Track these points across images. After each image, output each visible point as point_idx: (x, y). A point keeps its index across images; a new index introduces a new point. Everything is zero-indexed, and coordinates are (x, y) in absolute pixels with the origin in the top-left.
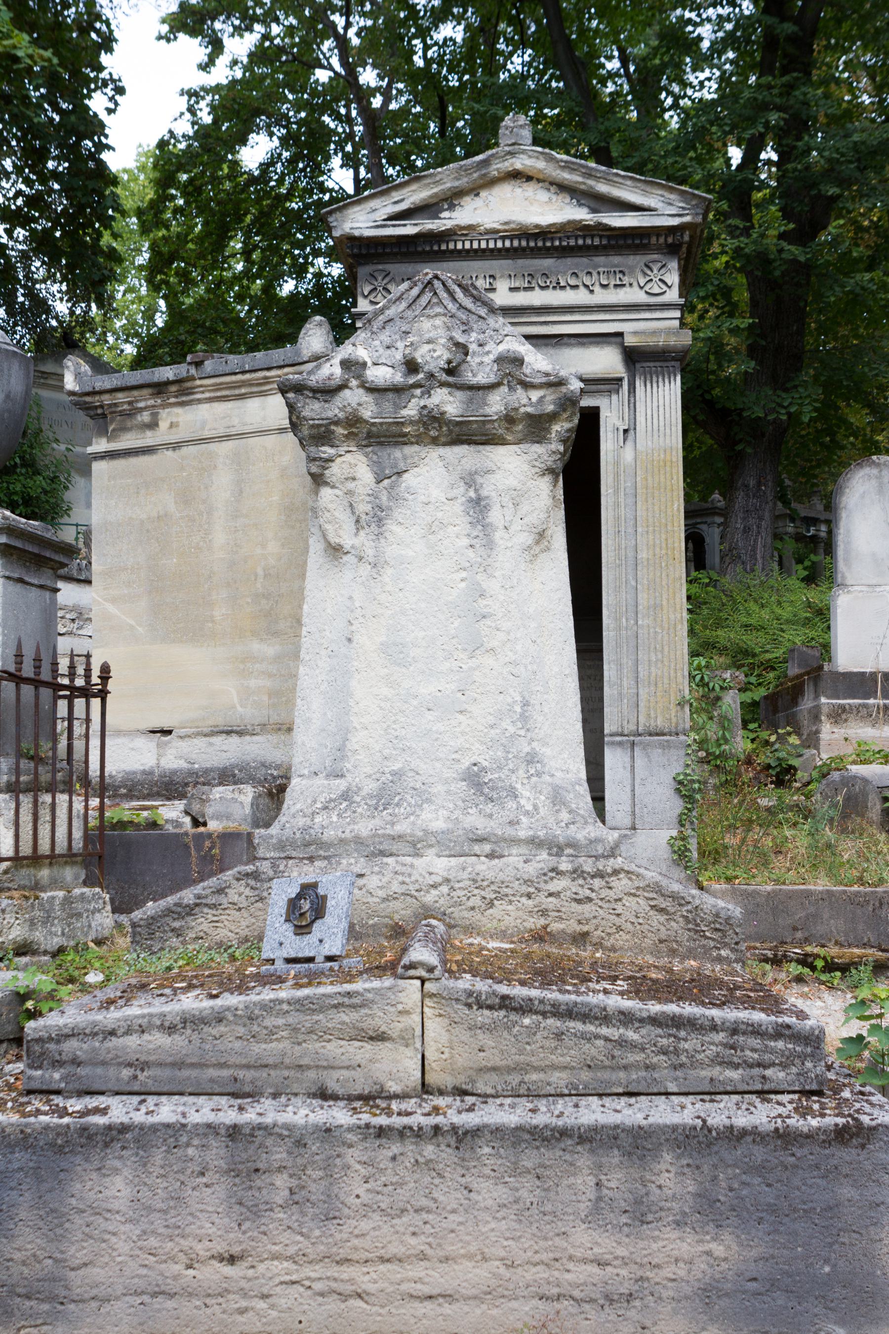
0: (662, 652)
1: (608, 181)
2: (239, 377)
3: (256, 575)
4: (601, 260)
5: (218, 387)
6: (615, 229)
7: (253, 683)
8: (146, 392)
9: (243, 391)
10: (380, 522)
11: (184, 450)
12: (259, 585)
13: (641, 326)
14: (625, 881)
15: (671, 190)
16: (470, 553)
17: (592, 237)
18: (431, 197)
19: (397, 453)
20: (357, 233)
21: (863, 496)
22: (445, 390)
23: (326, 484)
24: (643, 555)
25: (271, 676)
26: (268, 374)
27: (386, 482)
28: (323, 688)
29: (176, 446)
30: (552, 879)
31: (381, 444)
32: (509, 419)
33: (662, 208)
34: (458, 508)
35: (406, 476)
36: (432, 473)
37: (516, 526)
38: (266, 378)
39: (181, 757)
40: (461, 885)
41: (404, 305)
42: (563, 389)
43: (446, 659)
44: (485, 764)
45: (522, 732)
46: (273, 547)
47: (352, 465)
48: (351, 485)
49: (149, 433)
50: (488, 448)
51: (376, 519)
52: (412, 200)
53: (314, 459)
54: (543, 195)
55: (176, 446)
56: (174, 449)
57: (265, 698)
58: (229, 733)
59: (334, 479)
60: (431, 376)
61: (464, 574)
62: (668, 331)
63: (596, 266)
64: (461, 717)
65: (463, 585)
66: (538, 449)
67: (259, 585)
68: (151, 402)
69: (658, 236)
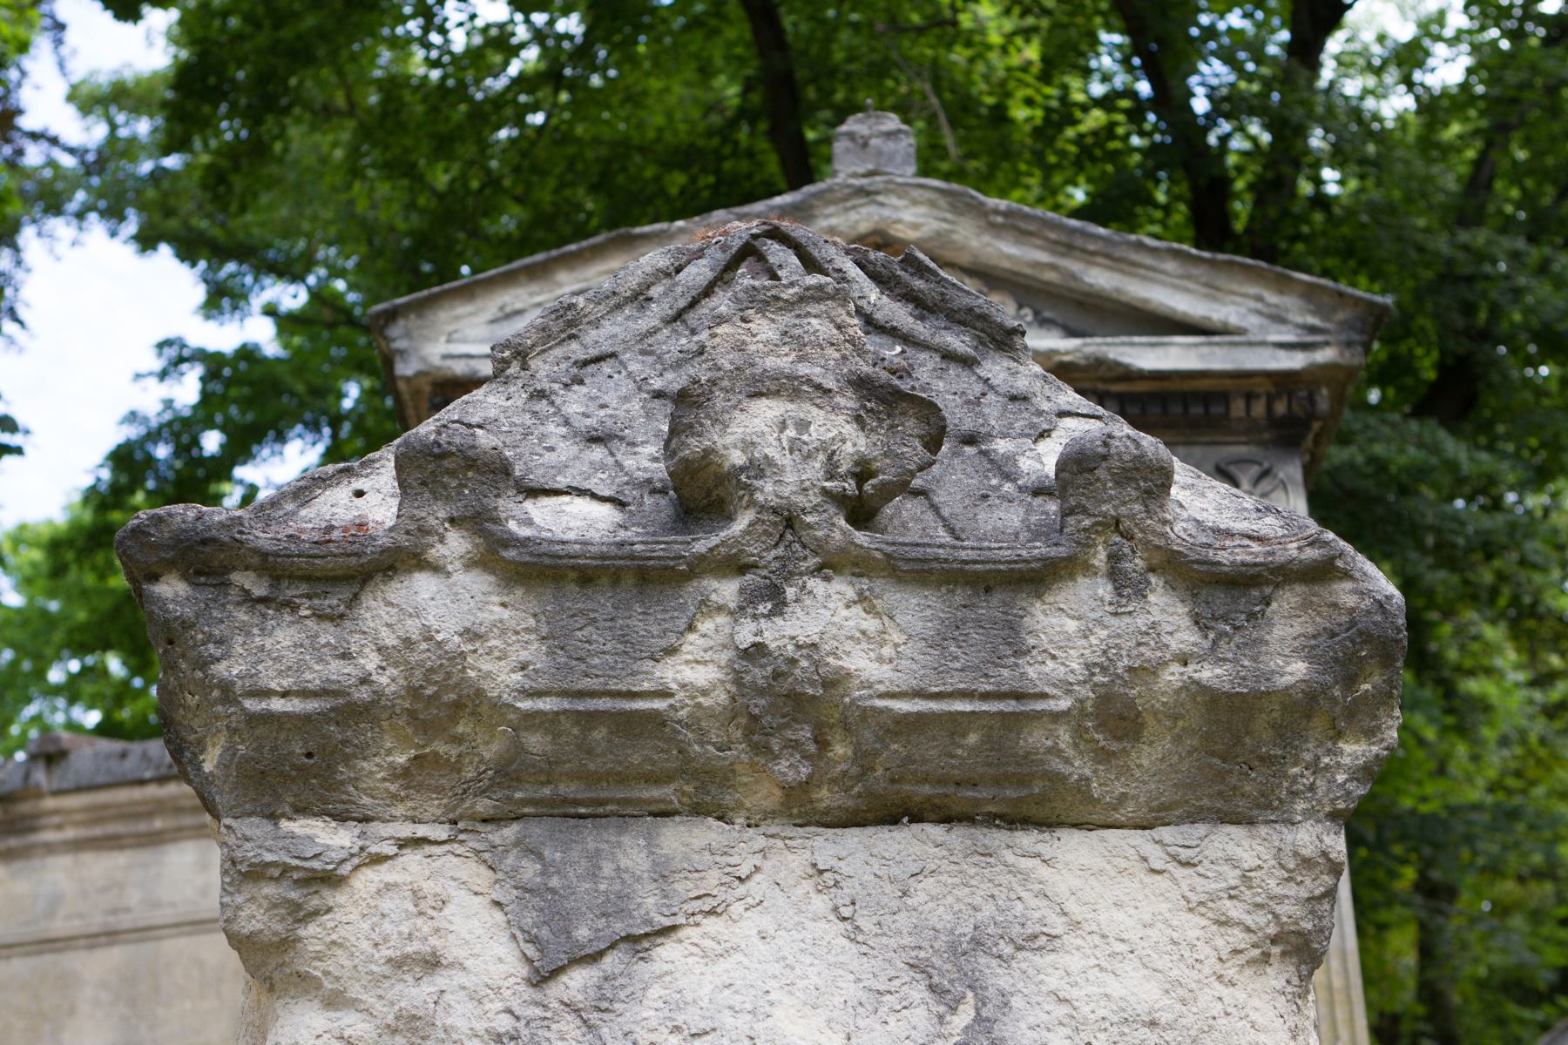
1: (1117, 263)
2: (152, 791)
5: (97, 815)
6: (1143, 376)
9: (158, 824)
19: (631, 853)
22: (843, 587)
23: (305, 985)
27: (577, 981)
31: (564, 811)
32: (1114, 715)
35: (667, 952)
41: (652, 317)
48: (415, 993)
50: (1027, 839)
53: (257, 873)
60: (788, 520)
66: (1240, 847)
69: (1249, 397)
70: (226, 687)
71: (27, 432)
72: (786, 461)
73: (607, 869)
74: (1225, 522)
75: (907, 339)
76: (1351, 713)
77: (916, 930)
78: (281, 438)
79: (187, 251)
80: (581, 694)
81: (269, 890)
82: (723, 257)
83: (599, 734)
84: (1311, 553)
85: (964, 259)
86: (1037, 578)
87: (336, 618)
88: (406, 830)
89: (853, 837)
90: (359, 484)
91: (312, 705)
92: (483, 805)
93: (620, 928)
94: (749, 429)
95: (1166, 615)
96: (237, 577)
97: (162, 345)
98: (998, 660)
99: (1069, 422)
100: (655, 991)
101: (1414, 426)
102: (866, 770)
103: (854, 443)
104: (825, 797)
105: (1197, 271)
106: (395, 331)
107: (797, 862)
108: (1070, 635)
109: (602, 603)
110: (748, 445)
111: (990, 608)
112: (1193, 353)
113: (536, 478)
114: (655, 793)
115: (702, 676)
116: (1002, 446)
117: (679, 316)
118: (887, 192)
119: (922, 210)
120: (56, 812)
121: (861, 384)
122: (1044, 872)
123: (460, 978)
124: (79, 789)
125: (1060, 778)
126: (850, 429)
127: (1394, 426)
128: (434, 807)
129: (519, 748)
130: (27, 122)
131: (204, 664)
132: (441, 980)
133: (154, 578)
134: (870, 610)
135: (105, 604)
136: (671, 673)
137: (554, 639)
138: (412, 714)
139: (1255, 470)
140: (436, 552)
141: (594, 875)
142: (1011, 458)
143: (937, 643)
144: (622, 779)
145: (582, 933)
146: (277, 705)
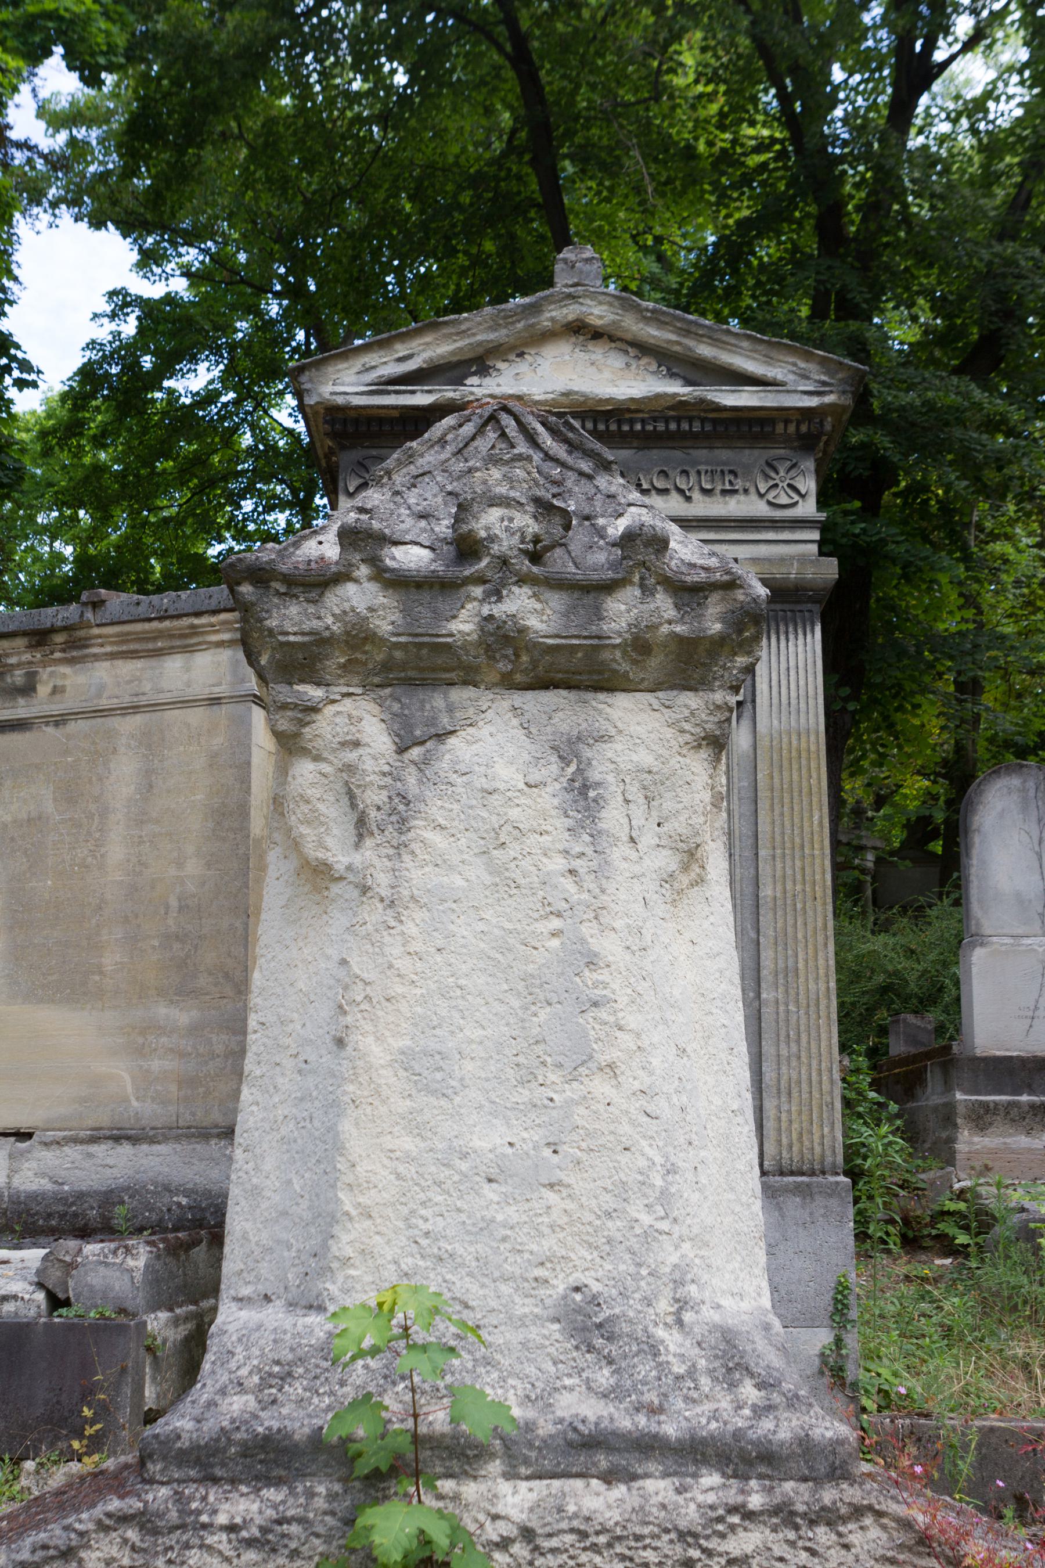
0: (798, 1041)
2: (155, 624)
3: (167, 907)
4: (702, 454)
5: (124, 639)
7: (156, 1065)
8: (20, 642)
10: (403, 824)
11: (72, 727)
12: (170, 922)
13: (763, 550)
14: (874, 1533)
15: (808, 356)
16: (568, 884)
17: (691, 420)
18: (453, 353)
19: (438, 701)
20: (340, 400)
21: (1001, 815)
22: (526, 590)
23: (304, 752)
24: (767, 891)
25: (182, 1055)
26: (196, 621)
27: (416, 752)
28: (284, 1130)
29: (59, 721)
30: (733, 1528)
31: (410, 683)
32: (640, 645)
33: (790, 381)
34: (550, 798)
35: (452, 741)
36: (495, 742)
37: (647, 840)
38: (193, 626)
39: (43, 1175)
40: (554, 1543)
42: (740, 595)
43: (522, 1083)
44: (596, 1287)
45: (664, 1225)
46: (193, 867)
47: (356, 721)
48: (351, 756)
49: (21, 701)
50: (602, 696)
51: (384, 819)
52: (427, 355)
54: (616, 361)
55: (59, 721)
56: (57, 724)
57: (173, 1088)
58: (117, 1139)
59: (319, 743)
60: (504, 562)
61: (556, 923)
62: (802, 559)
63: (695, 463)
64: (551, 1197)
65: (555, 943)
66: (691, 700)
67: (170, 922)
68: (27, 657)
69: (787, 422)
70: (270, 631)
71: (39, 372)
72: (503, 535)
73: (428, 707)
74: (695, 560)
75: (563, 465)
76: (740, 645)
77: (554, 733)
78: (194, 359)
79: (126, 229)
80: (417, 635)
81: (289, 713)
82: (480, 421)
83: (424, 651)
84: (726, 578)
85: (629, 337)
86: (609, 587)
87: (314, 602)
88: (345, 690)
89: (530, 695)
90: (320, 538)
91: (306, 639)
92: (377, 680)
93: (433, 731)
94: (490, 521)
95: (664, 604)
96: (273, 584)
97: (112, 294)
98: (591, 622)
99: (633, 509)
100: (447, 757)
101: (955, 380)
102: (535, 667)
103: (533, 527)
104: (518, 678)
105: (760, 348)
106: (303, 378)
107: (506, 704)
108: (622, 612)
109: (426, 596)
110: (487, 528)
111: (589, 600)
112: (755, 396)
113: (396, 537)
114: (448, 675)
115: (467, 627)
116: (601, 521)
117: (460, 451)
118: (585, 296)
119: (605, 307)
120: (100, 636)
121: (537, 501)
122: (608, 710)
123: (368, 750)
124: (112, 624)
125: (615, 672)
126: (531, 521)
127: (942, 378)
128: (356, 680)
129: (391, 657)
130: (13, 135)
131: (261, 620)
132: (360, 751)
133: (239, 584)
134: (539, 600)
135: (80, 474)
136: (455, 626)
137: (406, 611)
138: (347, 642)
139: (788, 464)
140: (356, 574)
141: (422, 709)
142: (604, 528)
143: (566, 615)
144: (434, 670)
145: (418, 733)
146: (292, 638)
